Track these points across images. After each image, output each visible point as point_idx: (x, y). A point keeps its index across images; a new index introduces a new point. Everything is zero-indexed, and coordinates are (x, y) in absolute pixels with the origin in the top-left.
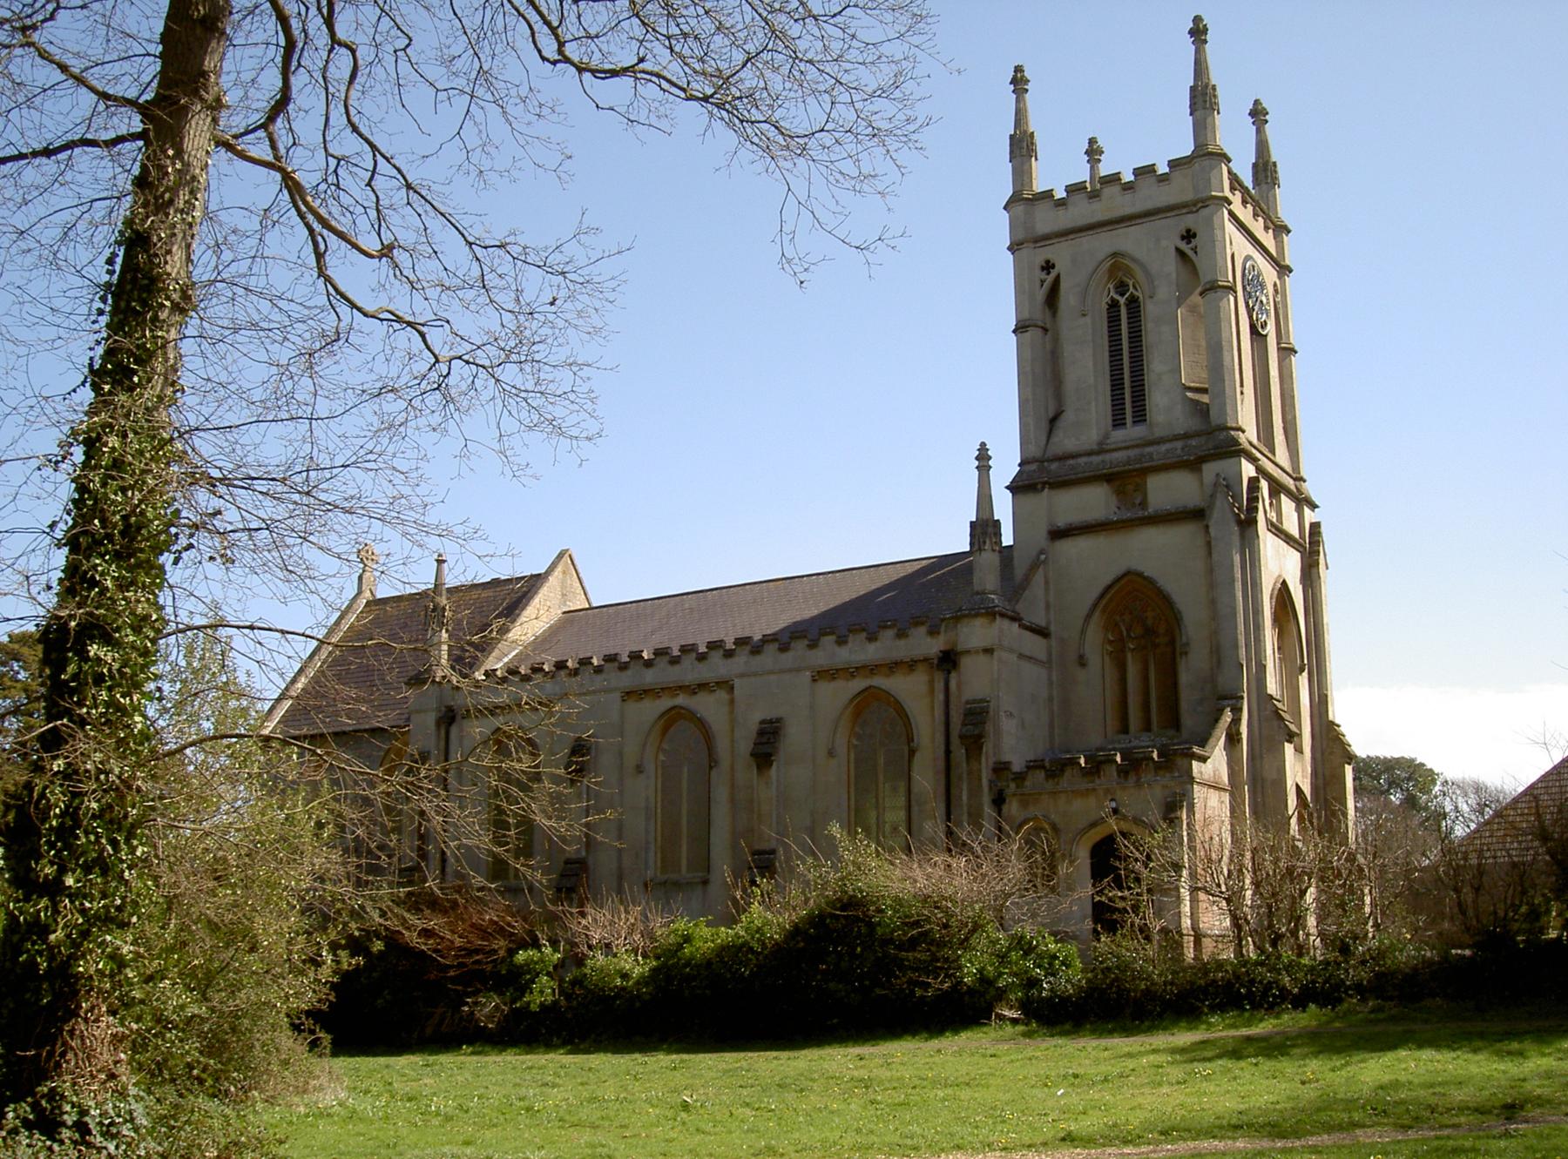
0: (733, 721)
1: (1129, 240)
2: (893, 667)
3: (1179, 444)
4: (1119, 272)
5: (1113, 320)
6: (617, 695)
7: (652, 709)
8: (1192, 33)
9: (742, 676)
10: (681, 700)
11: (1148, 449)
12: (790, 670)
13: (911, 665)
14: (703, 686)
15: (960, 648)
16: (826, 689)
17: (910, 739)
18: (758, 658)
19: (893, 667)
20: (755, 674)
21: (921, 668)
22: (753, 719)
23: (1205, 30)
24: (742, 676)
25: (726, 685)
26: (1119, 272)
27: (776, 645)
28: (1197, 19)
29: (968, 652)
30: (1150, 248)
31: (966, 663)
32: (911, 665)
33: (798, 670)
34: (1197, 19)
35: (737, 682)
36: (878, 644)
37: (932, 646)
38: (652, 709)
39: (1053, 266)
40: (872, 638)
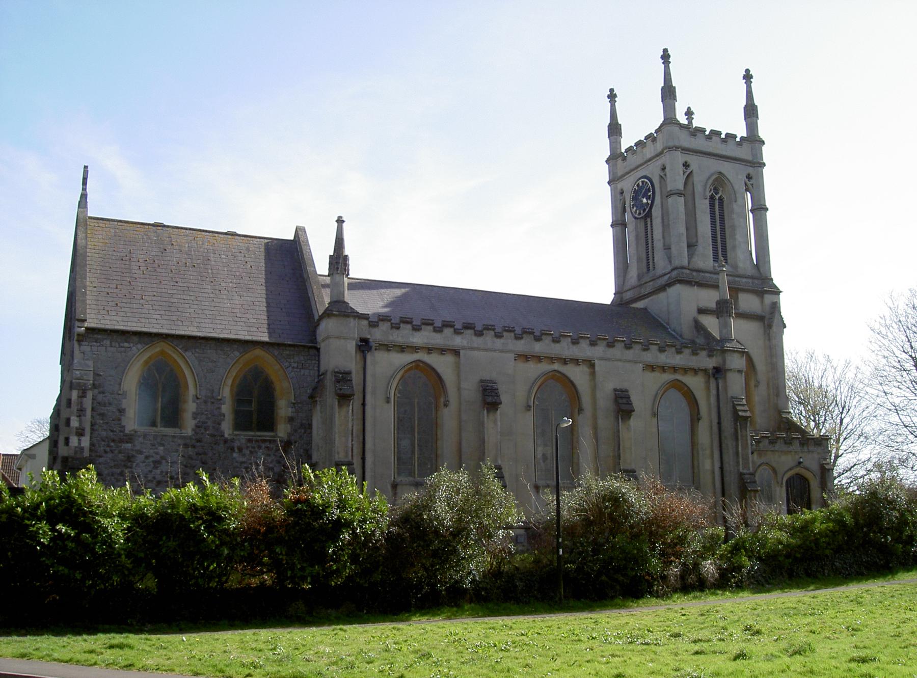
0: (594, 389)
1: (727, 168)
2: (685, 370)
3: (750, 281)
4: (719, 182)
5: (712, 206)
6: (512, 356)
7: (534, 370)
8: (662, 57)
9: (601, 359)
10: (556, 366)
11: (737, 279)
12: (629, 361)
13: (695, 371)
14: (576, 361)
15: (727, 367)
16: (650, 375)
17: (698, 413)
18: (611, 350)
19: (685, 370)
20: (609, 360)
21: (701, 374)
22: (608, 386)
23: (752, 77)
24: (601, 359)
25: (456, 353)
26: (719, 182)
27: (605, 343)
28: (747, 71)
29: (731, 370)
30: (735, 174)
31: (730, 375)
32: (695, 371)
33: (636, 362)
34: (747, 71)
35: (461, 352)
36: (681, 356)
37: (710, 363)
38: (534, 370)
39: (688, 166)
40: (679, 352)
